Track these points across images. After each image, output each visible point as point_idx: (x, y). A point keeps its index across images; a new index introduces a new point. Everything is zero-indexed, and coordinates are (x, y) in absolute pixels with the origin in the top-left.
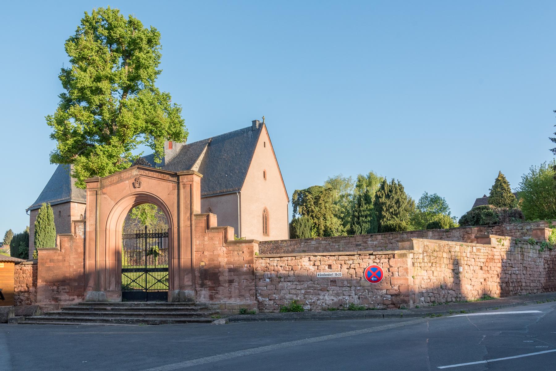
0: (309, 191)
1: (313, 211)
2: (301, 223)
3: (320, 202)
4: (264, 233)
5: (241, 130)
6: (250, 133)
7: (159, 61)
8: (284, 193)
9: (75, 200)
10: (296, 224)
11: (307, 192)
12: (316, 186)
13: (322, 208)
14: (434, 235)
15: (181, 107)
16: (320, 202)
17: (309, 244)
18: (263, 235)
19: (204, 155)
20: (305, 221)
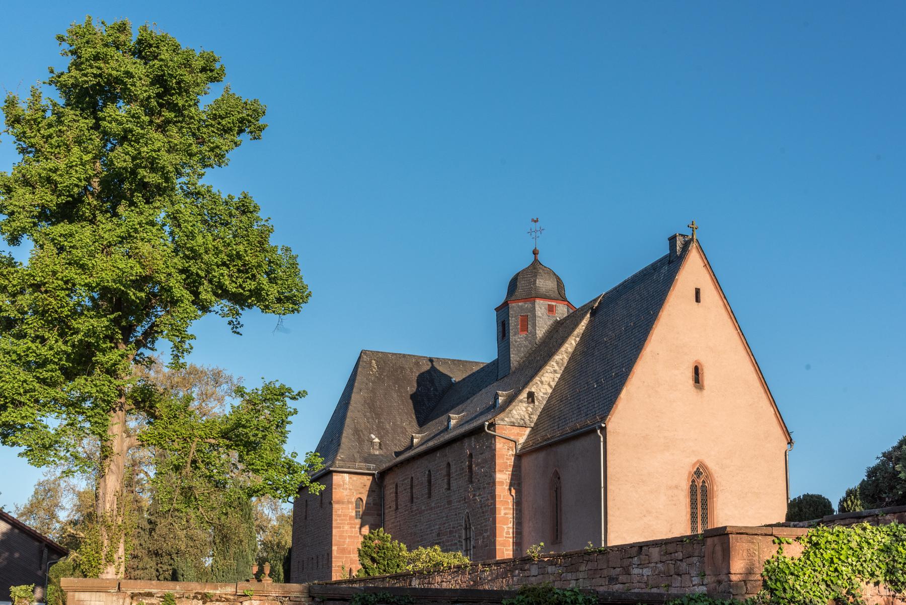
5: (652, 265)
9: (342, 467)
10: (852, 503)
15: (270, 223)
19: (578, 339)
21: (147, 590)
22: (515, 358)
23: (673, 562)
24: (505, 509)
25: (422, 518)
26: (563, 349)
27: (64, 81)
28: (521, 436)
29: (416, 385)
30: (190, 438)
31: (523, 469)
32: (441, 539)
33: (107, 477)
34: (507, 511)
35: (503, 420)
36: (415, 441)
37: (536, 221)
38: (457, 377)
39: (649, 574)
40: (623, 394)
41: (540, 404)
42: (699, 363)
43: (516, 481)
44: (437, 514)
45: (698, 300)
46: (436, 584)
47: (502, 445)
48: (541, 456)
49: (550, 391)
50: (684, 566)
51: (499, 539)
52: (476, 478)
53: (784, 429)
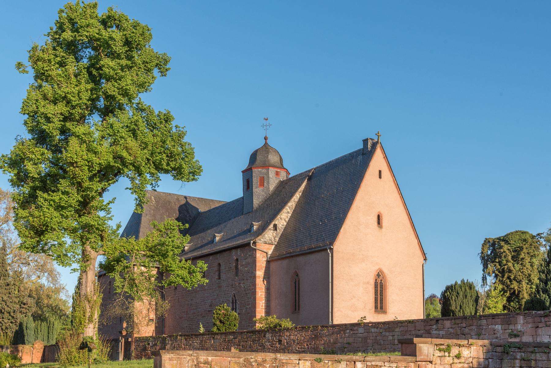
0: (505, 240)
1: (510, 271)
2: (459, 292)
3: (521, 257)
4: (376, 307)
5: (350, 154)
6: (360, 158)
7: (167, 67)
8: (417, 247)
10: (450, 294)
11: (503, 240)
12: (517, 232)
13: (525, 266)
14: (527, 322)
16: (521, 257)
17: (355, 332)
18: (375, 311)
19: (301, 194)
20: (465, 290)
21: (440, 343)
22: (256, 202)
23: (460, 328)
24: (261, 292)
25: (197, 295)
26: (292, 199)
27: (68, 38)
28: (270, 250)
29: (178, 212)
30: (132, 251)
31: (271, 269)
32: (212, 308)
33: (88, 272)
34: (262, 294)
35: (260, 240)
36: (186, 248)
37: (267, 120)
38: (202, 209)
39: (444, 333)
40: (342, 230)
41: (280, 230)
42: (380, 213)
43: (267, 276)
44: (210, 293)
45: (380, 177)
46: (285, 337)
47: (259, 255)
48: (285, 262)
49: (285, 224)
50: (466, 330)
51: (257, 310)
52: (241, 274)
53: (423, 252)
